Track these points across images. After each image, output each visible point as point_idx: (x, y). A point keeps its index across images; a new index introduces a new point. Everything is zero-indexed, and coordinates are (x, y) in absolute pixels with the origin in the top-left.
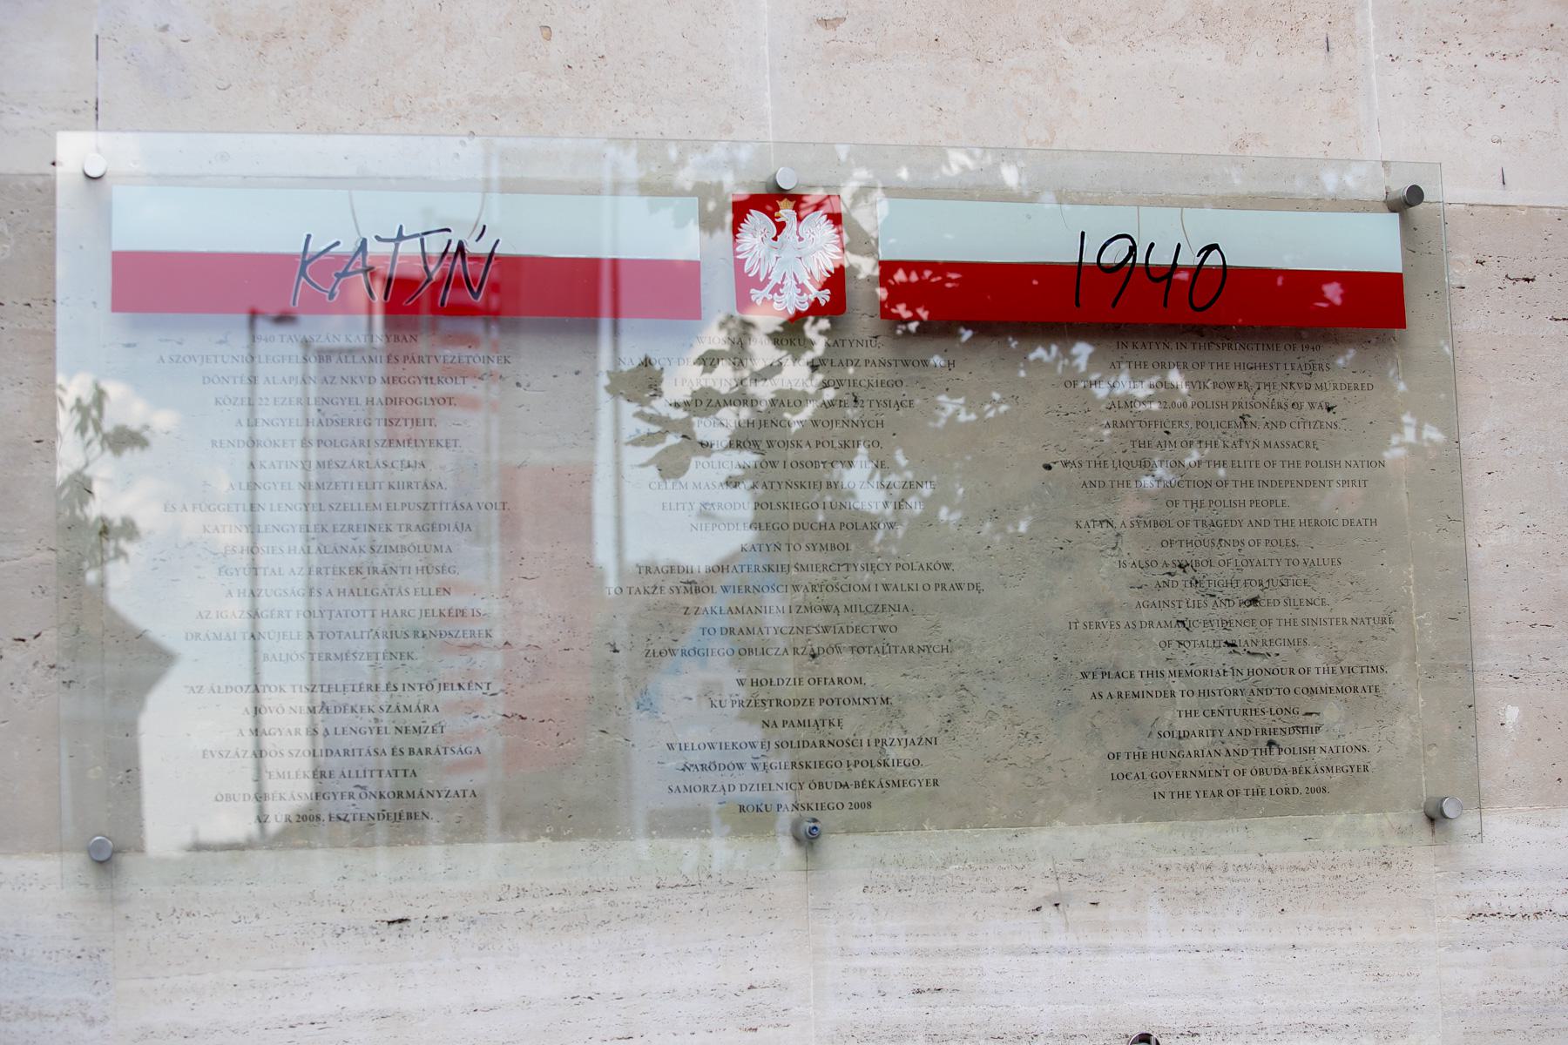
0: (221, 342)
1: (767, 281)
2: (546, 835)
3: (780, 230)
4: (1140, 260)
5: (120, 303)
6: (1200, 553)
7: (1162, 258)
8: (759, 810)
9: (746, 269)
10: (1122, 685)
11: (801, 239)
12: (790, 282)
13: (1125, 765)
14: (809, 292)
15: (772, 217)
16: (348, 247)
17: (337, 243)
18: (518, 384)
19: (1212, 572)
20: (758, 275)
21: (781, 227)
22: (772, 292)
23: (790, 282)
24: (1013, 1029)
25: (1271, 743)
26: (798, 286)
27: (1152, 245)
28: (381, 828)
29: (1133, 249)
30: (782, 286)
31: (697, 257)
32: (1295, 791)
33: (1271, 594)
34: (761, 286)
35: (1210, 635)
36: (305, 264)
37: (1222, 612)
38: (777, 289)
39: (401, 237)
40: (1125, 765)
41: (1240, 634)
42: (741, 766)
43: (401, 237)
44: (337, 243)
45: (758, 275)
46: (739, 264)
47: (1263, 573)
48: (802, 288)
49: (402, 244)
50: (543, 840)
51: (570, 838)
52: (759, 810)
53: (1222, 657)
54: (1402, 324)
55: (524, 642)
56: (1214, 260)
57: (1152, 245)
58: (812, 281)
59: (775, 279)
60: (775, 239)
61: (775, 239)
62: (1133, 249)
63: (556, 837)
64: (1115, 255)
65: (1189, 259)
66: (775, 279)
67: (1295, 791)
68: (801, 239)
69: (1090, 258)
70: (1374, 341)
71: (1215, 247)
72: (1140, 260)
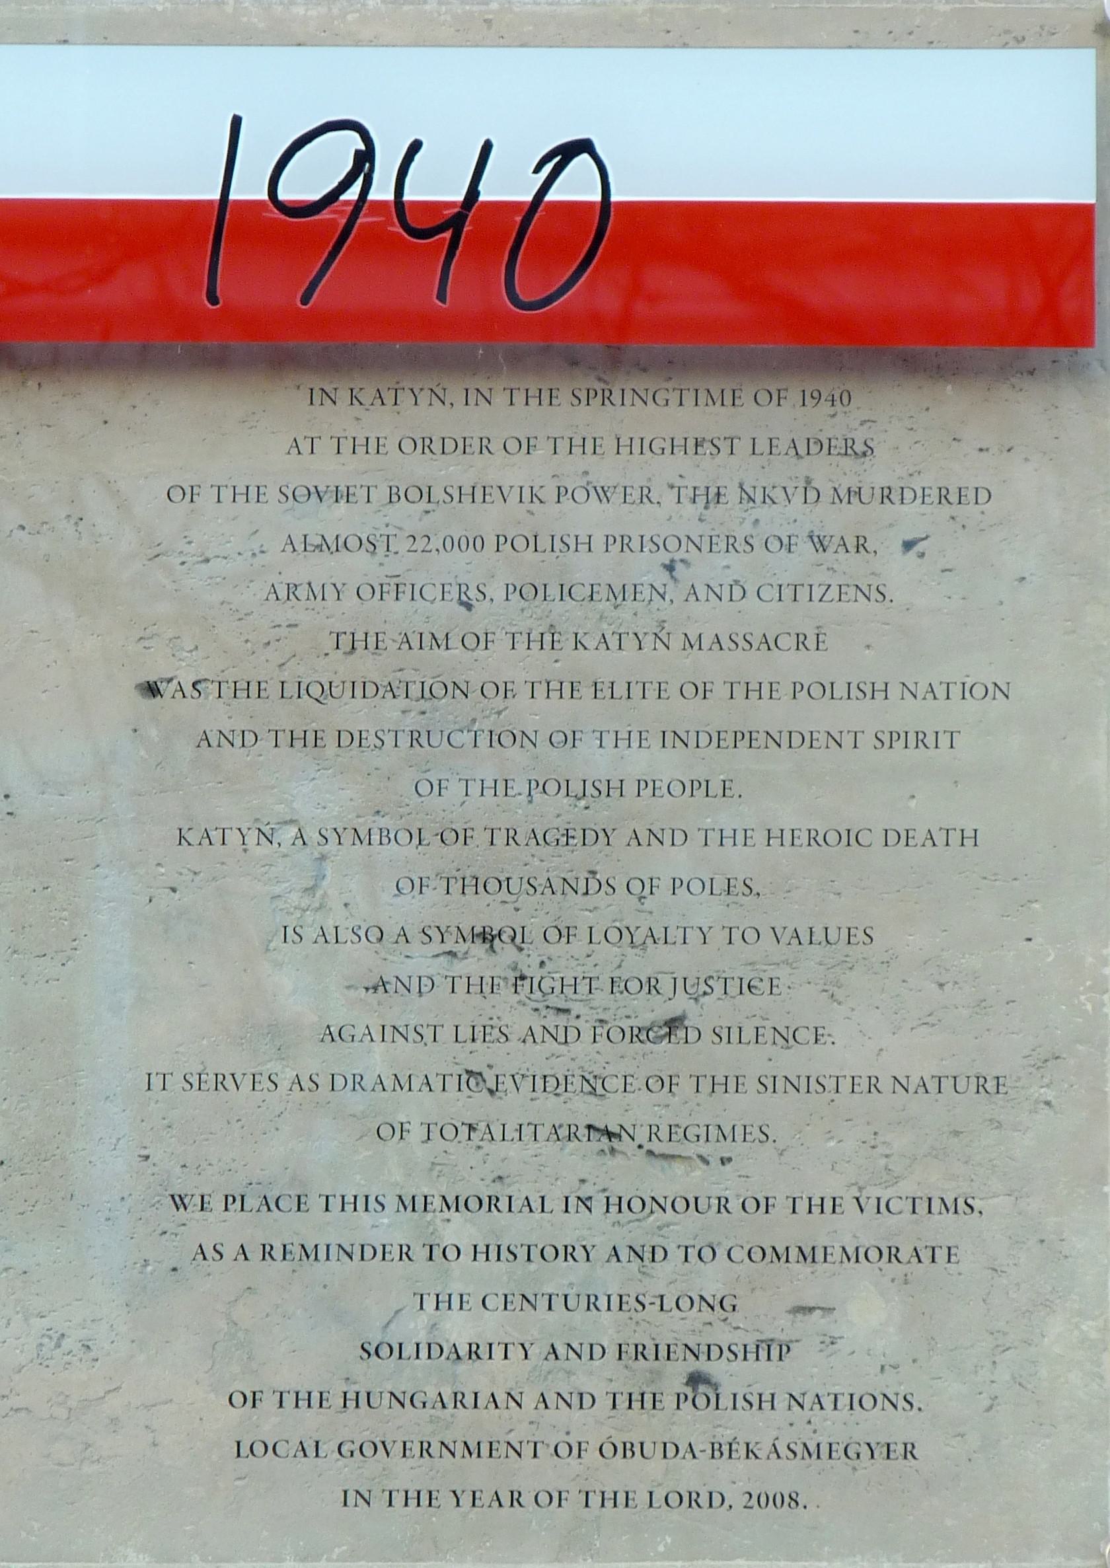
4: (383, 192)
6: (535, 914)
7: (437, 184)
10: (286, 1227)
13: (269, 1422)
19: (567, 960)
24: (557, 822)
25: (695, 1380)
27: (415, 147)
29: (365, 159)
33: (710, 1012)
37: (583, 1053)
40: (269, 1422)
41: (635, 1110)
53: (579, 1163)
56: (577, 185)
57: (415, 147)
62: (365, 159)
64: (313, 177)
65: (512, 184)
69: (250, 187)
70: (367, 396)
71: (584, 146)
72: (383, 192)
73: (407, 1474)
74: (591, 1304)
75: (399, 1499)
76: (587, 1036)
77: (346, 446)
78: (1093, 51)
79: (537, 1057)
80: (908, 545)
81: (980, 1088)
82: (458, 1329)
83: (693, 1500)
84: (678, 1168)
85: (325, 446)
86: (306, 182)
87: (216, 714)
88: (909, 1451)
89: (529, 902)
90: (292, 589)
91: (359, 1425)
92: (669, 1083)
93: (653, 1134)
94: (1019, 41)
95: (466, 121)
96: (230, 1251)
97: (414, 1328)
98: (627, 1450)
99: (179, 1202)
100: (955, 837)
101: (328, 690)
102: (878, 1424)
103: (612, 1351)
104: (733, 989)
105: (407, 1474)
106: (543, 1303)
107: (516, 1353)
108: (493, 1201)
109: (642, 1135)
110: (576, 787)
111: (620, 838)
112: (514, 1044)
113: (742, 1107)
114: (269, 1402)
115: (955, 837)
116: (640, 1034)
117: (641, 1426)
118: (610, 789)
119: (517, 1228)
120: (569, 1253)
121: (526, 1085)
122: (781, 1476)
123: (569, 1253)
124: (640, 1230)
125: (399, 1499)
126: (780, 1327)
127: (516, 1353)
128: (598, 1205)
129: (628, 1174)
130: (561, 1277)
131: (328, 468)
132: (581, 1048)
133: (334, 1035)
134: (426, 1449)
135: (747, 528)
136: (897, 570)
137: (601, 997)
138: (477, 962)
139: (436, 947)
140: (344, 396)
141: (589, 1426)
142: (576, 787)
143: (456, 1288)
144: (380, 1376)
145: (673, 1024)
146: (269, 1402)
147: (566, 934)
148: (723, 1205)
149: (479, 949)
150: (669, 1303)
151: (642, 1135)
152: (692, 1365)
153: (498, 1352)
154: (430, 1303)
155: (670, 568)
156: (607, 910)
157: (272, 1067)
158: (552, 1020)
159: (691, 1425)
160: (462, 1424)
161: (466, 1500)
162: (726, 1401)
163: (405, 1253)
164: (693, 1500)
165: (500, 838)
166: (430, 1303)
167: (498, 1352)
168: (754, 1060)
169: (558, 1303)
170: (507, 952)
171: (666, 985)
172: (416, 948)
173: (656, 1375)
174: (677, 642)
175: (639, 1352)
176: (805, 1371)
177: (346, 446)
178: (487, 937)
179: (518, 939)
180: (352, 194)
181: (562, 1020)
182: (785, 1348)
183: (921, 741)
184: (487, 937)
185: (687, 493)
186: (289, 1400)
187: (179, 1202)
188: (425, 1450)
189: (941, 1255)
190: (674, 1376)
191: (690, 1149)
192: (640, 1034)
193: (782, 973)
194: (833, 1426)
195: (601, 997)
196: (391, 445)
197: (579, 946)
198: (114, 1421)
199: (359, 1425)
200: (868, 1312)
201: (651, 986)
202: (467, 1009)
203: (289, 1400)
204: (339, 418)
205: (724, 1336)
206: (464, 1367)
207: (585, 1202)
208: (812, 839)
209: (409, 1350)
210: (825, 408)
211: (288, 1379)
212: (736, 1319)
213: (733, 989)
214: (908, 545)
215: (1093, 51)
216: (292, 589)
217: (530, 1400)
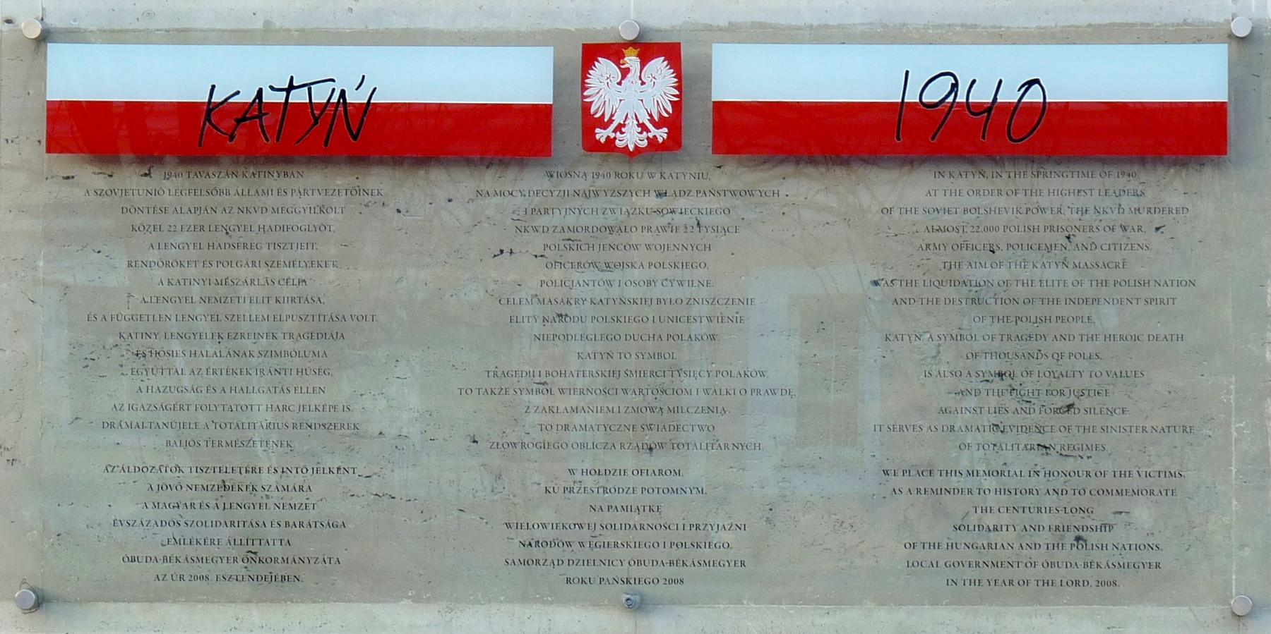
0: (146, 175)
1: (611, 121)
2: (409, 598)
3: (624, 77)
5: (55, 144)
7: (982, 96)
8: (583, 581)
9: (592, 111)
11: (643, 83)
12: (632, 123)
13: (1148, 556)
14: (648, 131)
15: (618, 64)
16: (247, 97)
17: (238, 93)
18: (399, 211)
20: (603, 115)
21: (625, 72)
22: (615, 131)
23: (632, 123)
25: (1078, 539)
26: (639, 125)
28: (244, 588)
29: (955, 86)
30: (624, 125)
31: (1222, 97)
32: (1086, 583)
33: (1085, 403)
34: (605, 126)
35: (1024, 439)
36: (209, 111)
37: (1036, 418)
38: (619, 128)
39: (291, 87)
40: (920, 554)
41: (1056, 439)
42: (569, 544)
43: (291, 87)
44: (238, 93)
45: (603, 115)
46: (586, 107)
47: (1077, 384)
48: (643, 128)
49: (293, 92)
50: (405, 602)
51: (428, 601)
52: (583, 581)
53: (1036, 458)
54: (1225, 153)
55: (395, 432)
56: (1034, 96)
57: (974, 82)
58: (652, 120)
59: (618, 119)
60: (620, 83)
61: (620, 83)
62: (955, 86)
63: (417, 599)
65: (1009, 96)
66: (618, 119)
67: (1086, 583)
68: (643, 83)
69: (912, 97)
70: (240, 174)
71: (1037, 81)
73: (971, 574)
74: (1039, 510)
75: (967, 583)
76: (1037, 411)
77: (948, 193)
78: (1226, 46)
79: (1018, 420)
80: (1157, 229)
81: (1184, 430)
82: (990, 520)
83: (1077, 583)
84: (1071, 459)
85: (940, 193)
86: (932, 96)
87: (898, 291)
88: (1158, 566)
89: (1015, 362)
90: (928, 246)
91: (952, 556)
92: (1068, 429)
93: (1062, 447)
94: (1199, 41)
95: (992, 75)
96: (905, 491)
97: (973, 519)
98: (639, 563)
99: (886, 473)
100: (1175, 338)
101: (941, 283)
102: (1148, 556)
103: (1047, 528)
104: (1092, 393)
105: (971, 574)
106: (1021, 510)
107: (1011, 528)
108: (1002, 473)
109: (1058, 448)
110: (1033, 319)
111: (1049, 339)
112: (1010, 414)
113: (1093, 438)
114: (919, 546)
115: (1175, 338)
116: (1057, 411)
117: (1059, 556)
118: (1046, 320)
119: (1012, 483)
120: (1031, 492)
121: (1015, 430)
122: (1107, 575)
123: (1031, 492)
124: (1058, 483)
125: (967, 583)
126: (1111, 519)
127: (1011, 528)
128: (1042, 474)
129: (1050, 462)
130: (1029, 501)
131: (941, 201)
132: (1035, 416)
133: (944, 411)
134: (977, 564)
135: (1097, 223)
136: (1155, 239)
137: (1043, 397)
138: (997, 384)
139: (981, 378)
140: (240, 174)
141: (1039, 555)
142: (1033, 319)
143: (989, 504)
144: (963, 538)
145: (1070, 407)
146: (919, 546)
147: (1029, 373)
148: (1088, 474)
149: (997, 379)
150: (1068, 510)
151: (1058, 448)
152: (1077, 533)
153: (1004, 528)
154: (979, 511)
155: (1068, 238)
156: (1047, 364)
157: (920, 423)
158: (1025, 405)
159: (1078, 555)
160: (991, 556)
161: (992, 583)
162: (1089, 547)
163: (970, 492)
164: (1077, 583)
165: (1005, 338)
166: (979, 511)
167: (1004, 528)
168: (1097, 420)
169: (1027, 510)
170: (1007, 380)
171: (1067, 392)
172: (973, 379)
173: (1062, 537)
174: (1071, 266)
175: (1057, 528)
176: (1118, 535)
177: (948, 193)
178: (1001, 375)
179: (1012, 376)
180: (950, 99)
181: (1028, 405)
182: (1111, 527)
183: (1162, 302)
184: (1001, 375)
185: (1074, 211)
186: (927, 546)
187: (886, 473)
188: (977, 564)
189: (1170, 493)
190: (1070, 537)
191: (1076, 453)
192: (1057, 411)
193: (1110, 388)
194: (1131, 556)
195: (1043, 397)
196: (964, 192)
197: (1035, 377)
198: (862, 553)
199: (952, 556)
200: (1143, 514)
201: (1061, 393)
202: (993, 401)
203: (927, 546)
204: (945, 182)
205: (1089, 523)
206: (992, 534)
207: (1037, 473)
208: (1121, 338)
209: (971, 528)
210: (1126, 178)
211: (927, 539)
212: (1093, 516)
213: (1092, 393)
214: (1157, 229)
215: (1226, 46)
216: (928, 246)
217: (1016, 546)
